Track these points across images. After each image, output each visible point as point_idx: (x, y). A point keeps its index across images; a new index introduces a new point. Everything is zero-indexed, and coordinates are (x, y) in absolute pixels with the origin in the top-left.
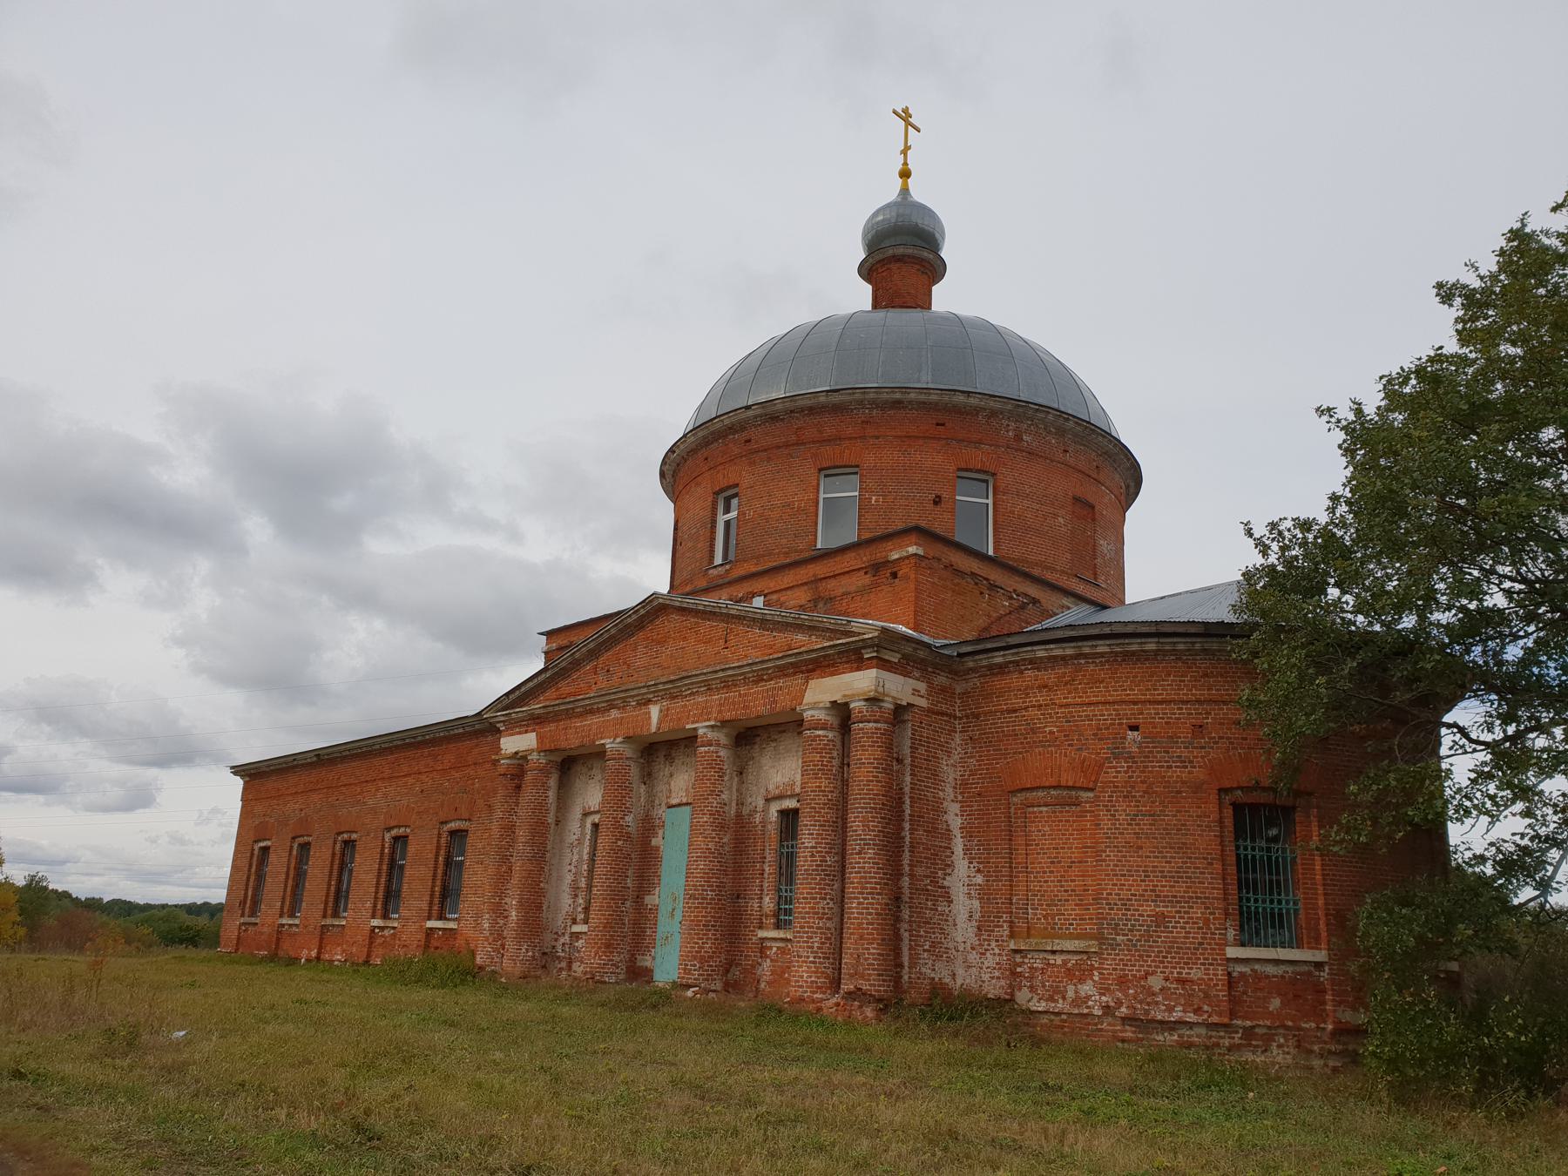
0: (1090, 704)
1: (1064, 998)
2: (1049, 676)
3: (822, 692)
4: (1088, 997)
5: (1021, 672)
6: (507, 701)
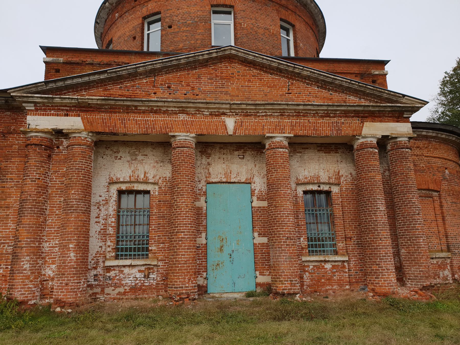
0: (435, 157)
1: (439, 277)
3: (373, 130)
4: (447, 276)
6: (45, 88)
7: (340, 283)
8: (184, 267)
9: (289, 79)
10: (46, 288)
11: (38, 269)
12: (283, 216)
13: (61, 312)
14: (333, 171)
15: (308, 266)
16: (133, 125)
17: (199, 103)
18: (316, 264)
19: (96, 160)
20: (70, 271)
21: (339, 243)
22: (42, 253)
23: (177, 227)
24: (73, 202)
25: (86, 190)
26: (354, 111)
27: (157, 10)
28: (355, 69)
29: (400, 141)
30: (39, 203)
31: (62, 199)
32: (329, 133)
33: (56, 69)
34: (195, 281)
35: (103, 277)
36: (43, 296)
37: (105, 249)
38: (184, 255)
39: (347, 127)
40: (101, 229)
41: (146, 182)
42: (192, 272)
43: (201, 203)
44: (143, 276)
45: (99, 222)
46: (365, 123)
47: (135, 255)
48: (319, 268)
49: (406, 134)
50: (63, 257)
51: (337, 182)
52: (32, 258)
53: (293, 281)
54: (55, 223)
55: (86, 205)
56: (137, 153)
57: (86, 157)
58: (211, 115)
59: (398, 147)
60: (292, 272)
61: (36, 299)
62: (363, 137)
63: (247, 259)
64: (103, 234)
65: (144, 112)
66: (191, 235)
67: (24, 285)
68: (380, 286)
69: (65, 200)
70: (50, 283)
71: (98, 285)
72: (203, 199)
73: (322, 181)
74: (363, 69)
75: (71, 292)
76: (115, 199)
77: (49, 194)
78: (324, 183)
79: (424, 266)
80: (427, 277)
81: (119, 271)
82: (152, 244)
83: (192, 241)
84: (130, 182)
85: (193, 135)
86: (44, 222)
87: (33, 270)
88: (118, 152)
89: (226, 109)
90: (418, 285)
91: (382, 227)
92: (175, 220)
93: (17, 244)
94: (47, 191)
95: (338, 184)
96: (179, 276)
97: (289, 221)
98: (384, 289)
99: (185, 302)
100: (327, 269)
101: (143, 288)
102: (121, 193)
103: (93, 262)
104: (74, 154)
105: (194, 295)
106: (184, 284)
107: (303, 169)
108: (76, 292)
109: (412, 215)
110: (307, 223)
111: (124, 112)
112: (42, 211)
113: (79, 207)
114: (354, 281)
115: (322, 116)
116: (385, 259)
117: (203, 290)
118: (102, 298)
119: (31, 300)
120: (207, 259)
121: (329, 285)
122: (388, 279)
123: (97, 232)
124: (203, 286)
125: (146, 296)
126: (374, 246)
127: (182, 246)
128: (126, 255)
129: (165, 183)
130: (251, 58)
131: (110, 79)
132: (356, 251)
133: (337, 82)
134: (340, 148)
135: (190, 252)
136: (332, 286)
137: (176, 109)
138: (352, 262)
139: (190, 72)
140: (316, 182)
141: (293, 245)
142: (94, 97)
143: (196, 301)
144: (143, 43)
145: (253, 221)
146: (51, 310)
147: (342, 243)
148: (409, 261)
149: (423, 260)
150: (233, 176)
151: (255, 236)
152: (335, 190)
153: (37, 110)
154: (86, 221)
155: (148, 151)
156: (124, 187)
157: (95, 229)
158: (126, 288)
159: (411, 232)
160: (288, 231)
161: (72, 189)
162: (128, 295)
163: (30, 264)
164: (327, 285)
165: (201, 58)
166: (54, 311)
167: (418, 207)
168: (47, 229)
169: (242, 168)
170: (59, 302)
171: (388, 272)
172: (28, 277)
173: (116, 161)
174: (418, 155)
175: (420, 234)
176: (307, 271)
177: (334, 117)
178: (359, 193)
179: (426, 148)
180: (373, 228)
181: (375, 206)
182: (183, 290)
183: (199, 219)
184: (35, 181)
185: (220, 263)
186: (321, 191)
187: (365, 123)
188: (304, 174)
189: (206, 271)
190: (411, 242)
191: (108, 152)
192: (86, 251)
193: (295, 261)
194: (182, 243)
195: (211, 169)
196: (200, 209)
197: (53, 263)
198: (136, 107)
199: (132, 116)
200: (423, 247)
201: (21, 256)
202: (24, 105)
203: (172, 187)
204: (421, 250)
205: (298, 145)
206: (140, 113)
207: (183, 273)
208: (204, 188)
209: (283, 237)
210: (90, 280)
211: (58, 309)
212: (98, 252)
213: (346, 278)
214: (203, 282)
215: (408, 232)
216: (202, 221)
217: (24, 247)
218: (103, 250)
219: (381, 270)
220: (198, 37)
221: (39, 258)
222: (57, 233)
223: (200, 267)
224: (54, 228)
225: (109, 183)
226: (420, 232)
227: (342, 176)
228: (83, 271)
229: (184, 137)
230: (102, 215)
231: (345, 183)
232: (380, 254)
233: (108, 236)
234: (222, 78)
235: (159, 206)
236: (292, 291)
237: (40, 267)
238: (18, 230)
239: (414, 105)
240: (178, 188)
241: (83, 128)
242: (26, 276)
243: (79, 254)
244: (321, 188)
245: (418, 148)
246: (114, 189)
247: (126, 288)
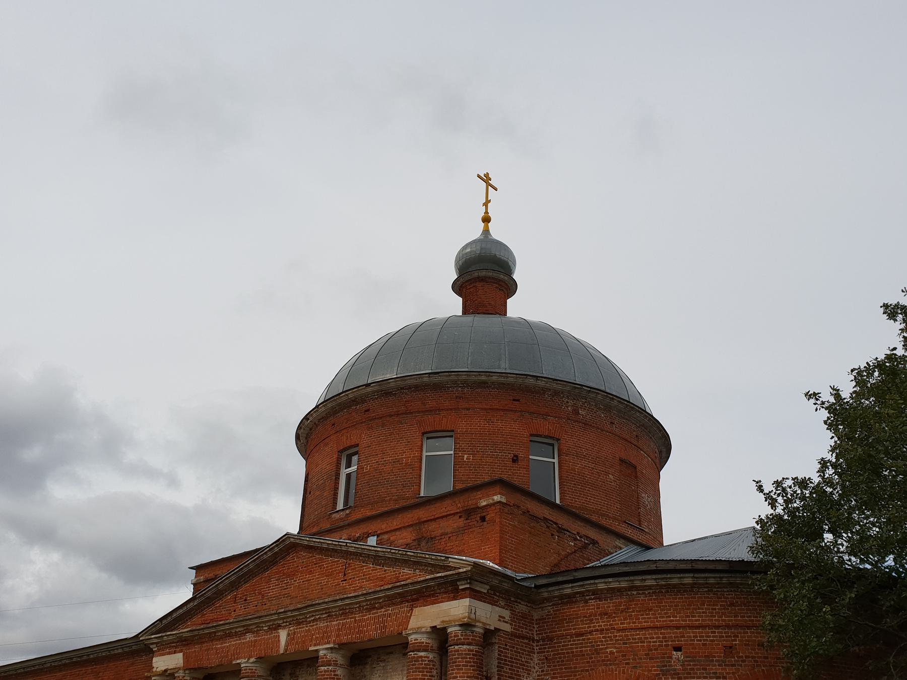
2: (608, 605)
49: (455, 621)
165: (265, 557)
174: (603, 630)
206: (219, 640)
245: (606, 614)
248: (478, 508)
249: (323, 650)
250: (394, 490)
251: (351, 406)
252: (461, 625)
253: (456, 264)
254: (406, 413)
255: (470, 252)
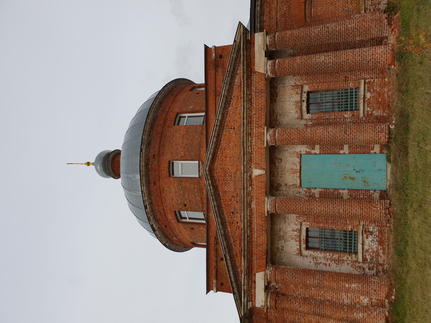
2: (267, 10)
3: (261, 65)
5: (264, 21)
6: (237, 295)
7: (382, 86)
8: (365, 210)
9: (224, 128)
10: (378, 303)
11: (363, 308)
12: (328, 136)
13: (395, 297)
14: (291, 91)
15: (368, 111)
16: (260, 239)
17: (244, 194)
18: (366, 105)
19: (284, 264)
20: (365, 288)
21: (349, 86)
22: (351, 304)
23: (335, 214)
24: (315, 282)
25: (307, 273)
26: (247, 80)
27: (173, 213)
28: (212, 72)
29: (269, 43)
30: (316, 304)
31: (313, 288)
32: (263, 99)
33: (221, 285)
34: (376, 202)
35: (371, 264)
36: (383, 306)
37: (350, 261)
38: (356, 210)
39: (259, 85)
40: (335, 263)
41: (300, 231)
42: (369, 204)
43: (316, 192)
44: (371, 236)
45: (330, 264)
46: (256, 70)
47: (355, 240)
48: (370, 102)
49: (264, 37)
50: (355, 291)
51: (300, 88)
52: (355, 311)
53: (379, 131)
54: (330, 295)
55: (318, 274)
56: (278, 235)
57: (284, 272)
58: (251, 185)
59: (273, 43)
60: (372, 131)
61: (385, 311)
62: (267, 72)
63: (361, 160)
64: (338, 261)
65: (251, 231)
66: (341, 204)
67: (374, 318)
68: (386, 60)
69: (314, 287)
70: (374, 301)
71: (377, 268)
72: (313, 191)
73: (299, 100)
74: (211, 67)
75: (381, 289)
76: (312, 252)
77: (310, 296)
78: (301, 97)
79: (371, 24)
80: (381, 22)
81: (366, 252)
82: (347, 228)
83: (346, 204)
84: (300, 241)
85: (266, 198)
86: (330, 302)
87: (363, 312)
88: (278, 248)
89: (247, 175)
90: (387, 29)
91: (338, 58)
92: (330, 215)
93: (345, 320)
94: (307, 298)
95: (302, 86)
96: (372, 214)
97: (332, 131)
98: (389, 58)
99: (395, 201)
100: (370, 97)
101: (380, 236)
102: (307, 248)
103: (359, 270)
104: (282, 279)
105: (387, 204)
106: (378, 210)
107: (290, 114)
108: (381, 285)
109: (328, 33)
110: (333, 111)
111: (252, 245)
112: (322, 302)
113: (319, 279)
114: (381, 75)
115: (251, 105)
116: (364, 56)
117: (384, 195)
118: (386, 266)
119: (385, 314)
120: (360, 190)
121: (384, 95)
122: (381, 54)
123: (337, 266)
124: (381, 193)
125: (386, 234)
126: (353, 65)
127: (350, 211)
128: (355, 246)
129: (301, 218)
130: (211, 156)
131: (230, 252)
132: (357, 73)
133: (226, 94)
134: (274, 85)
135: (354, 205)
136: (385, 92)
137: (248, 209)
138: (366, 77)
139: (222, 198)
140: (300, 104)
141: (351, 129)
142: (243, 264)
143: (392, 203)
144: (196, 223)
145: (331, 154)
146: (393, 302)
147: (349, 83)
148: (366, 35)
149: (366, 25)
150: (295, 168)
151: (343, 152)
152: (306, 88)
153: (252, 301)
154: (329, 274)
155: (277, 227)
156: (304, 246)
157: (334, 268)
158: (379, 248)
159: (343, 34)
160: (340, 133)
161: (306, 282)
162: (385, 248)
163: (359, 313)
164: (384, 96)
165: (212, 191)
166: (394, 300)
167: (322, 28)
168: (335, 300)
169: (289, 160)
170: (388, 296)
171: (375, 54)
172: (369, 315)
173: (285, 250)
175: (345, 27)
176: (372, 112)
177: (251, 95)
178: (310, 73)
179: (270, 5)
180: (338, 65)
181: (321, 64)
182: (383, 212)
183: (328, 194)
184: (301, 305)
185: (363, 180)
186: (307, 100)
187: (256, 70)
188: (294, 114)
189: (369, 190)
190: (351, 34)
191: (278, 255)
192: (351, 276)
193: (363, 128)
194: (348, 211)
195: (290, 184)
196: (321, 193)
197: (359, 298)
198: (248, 237)
199: (254, 239)
200: (355, 25)
201: (353, 318)
202: (249, 308)
203: (306, 215)
204: (358, 26)
205: (272, 122)
206: (252, 234)
207: (369, 212)
208: (304, 190)
209: (344, 137)
210: (373, 273)
211: (393, 297)
212: (351, 266)
213: (378, 81)
214: (377, 193)
215: (343, 36)
216: (330, 192)
217: (347, 315)
218: (350, 262)
219: (373, 59)
220: (192, 187)
221: (355, 307)
222: (338, 293)
223: (365, 195)
224: (334, 295)
225: (301, 255)
226: (343, 27)
227: (295, 83)
228: (365, 279)
229: (268, 205)
230: (324, 262)
231: (301, 81)
232: (360, 60)
233: (340, 259)
234: (225, 176)
235: (318, 222)
236: (387, 132)
237: (361, 307)
238: (335, 319)
239: (242, 33)
240: (306, 212)
241: (263, 272)
242: (368, 316)
243: (353, 281)
244: (305, 99)
245: (270, 12)
246: (306, 253)
247: (379, 248)
248: (215, 59)
249: (267, 137)
250: (197, 136)
251: (148, 168)
252: (267, 35)
253: (102, 176)
254: (162, 134)
255: (100, 166)
